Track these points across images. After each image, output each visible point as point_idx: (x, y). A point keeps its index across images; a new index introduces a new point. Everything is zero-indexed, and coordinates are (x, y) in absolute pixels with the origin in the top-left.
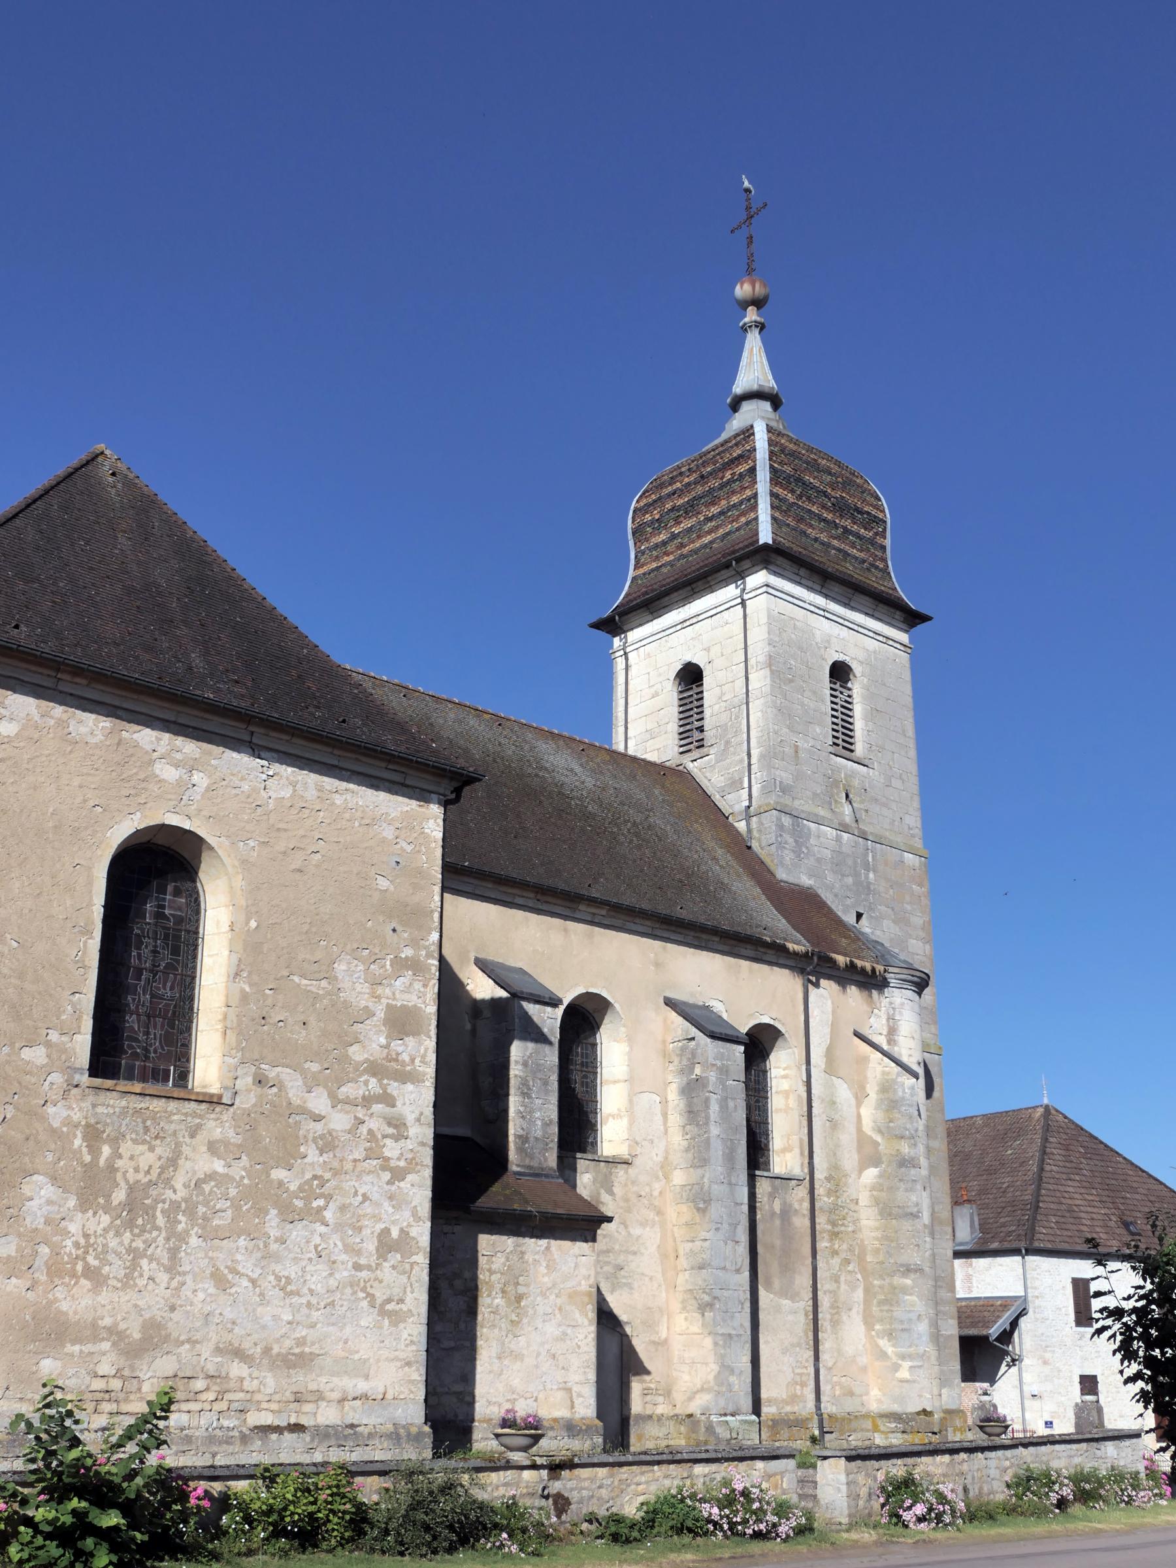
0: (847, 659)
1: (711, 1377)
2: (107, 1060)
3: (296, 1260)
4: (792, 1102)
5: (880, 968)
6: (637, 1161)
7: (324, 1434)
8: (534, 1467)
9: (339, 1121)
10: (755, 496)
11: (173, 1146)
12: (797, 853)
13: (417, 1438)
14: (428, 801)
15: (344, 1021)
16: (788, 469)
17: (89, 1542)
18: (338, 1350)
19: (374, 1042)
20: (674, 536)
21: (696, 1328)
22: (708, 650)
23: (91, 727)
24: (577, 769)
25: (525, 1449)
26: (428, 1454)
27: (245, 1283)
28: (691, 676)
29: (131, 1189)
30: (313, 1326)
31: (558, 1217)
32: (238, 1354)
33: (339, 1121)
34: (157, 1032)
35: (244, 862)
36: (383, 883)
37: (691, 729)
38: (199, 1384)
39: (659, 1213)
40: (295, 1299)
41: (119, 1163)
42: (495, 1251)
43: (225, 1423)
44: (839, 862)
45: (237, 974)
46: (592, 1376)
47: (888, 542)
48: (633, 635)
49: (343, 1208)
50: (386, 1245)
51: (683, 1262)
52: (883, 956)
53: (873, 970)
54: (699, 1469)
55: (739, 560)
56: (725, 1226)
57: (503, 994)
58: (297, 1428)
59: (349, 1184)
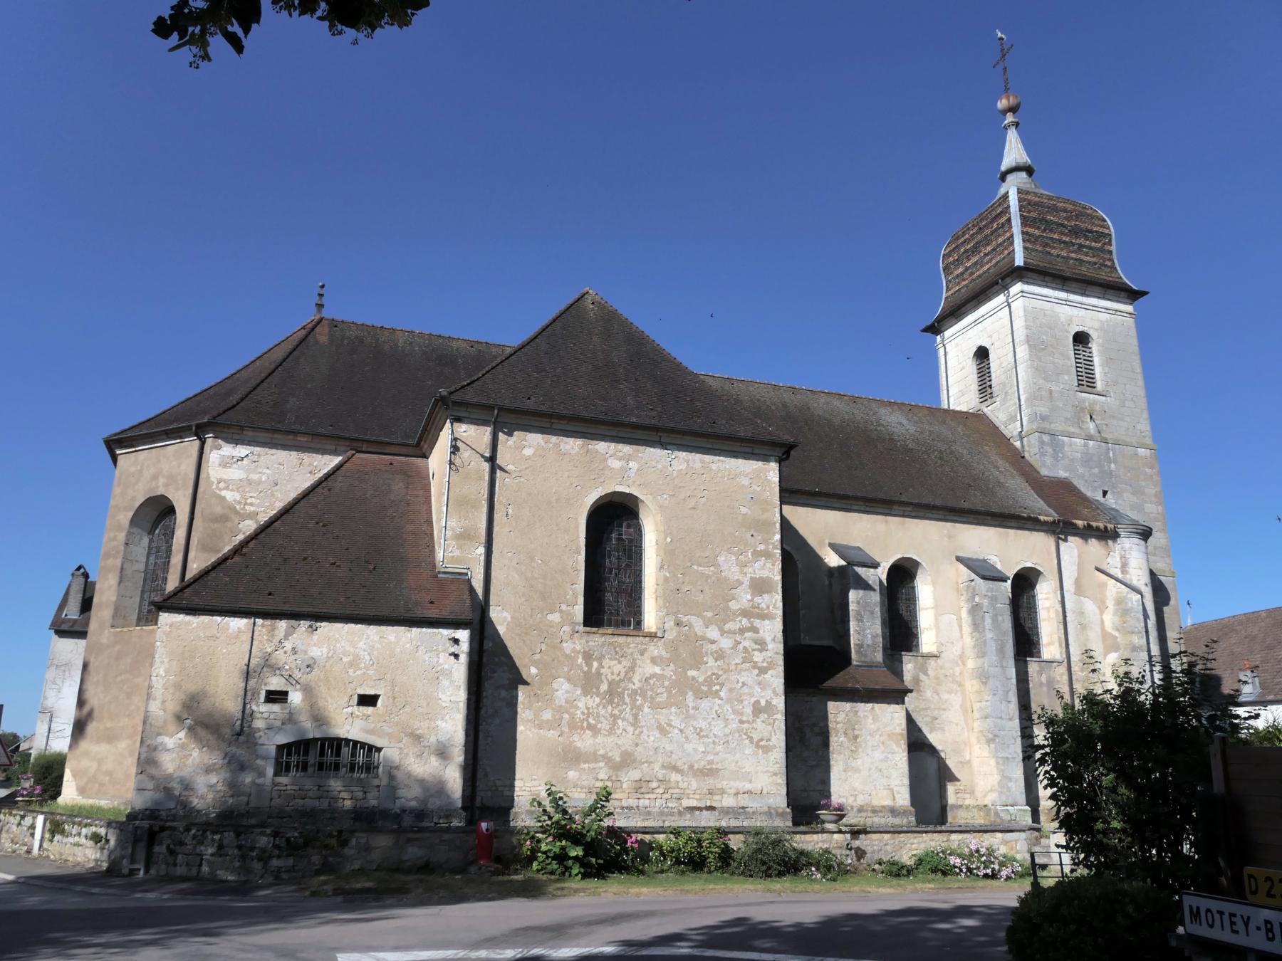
0: (1085, 329)
1: (995, 783)
2: (595, 615)
3: (705, 719)
4: (1052, 615)
5: (1110, 526)
6: (943, 655)
7: (727, 812)
8: (840, 832)
9: (726, 643)
10: (1012, 236)
11: (631, 660)
12: (1056, 458)
13: (782, 815)
14: (768, 461)
15: (726, 588)
16: (1034, 215)
17: (570, 862)
18: (733, 767)
19: (744, 598)
20: (967, 269)
21: (986, 754)
22: (990, 337)
23: (572, 445)
24: (904, 422)
25: (835, 822)
26: (790, 824)
27: (676, 731)
28: (982, 354)
29: (610, 684)
30: (717, 754)
31: (876, 690)
32: (675, 768)
33: (726, 643)
34: (622, 601)
35: (661, 507)
36: (744, 510)
37: (985, 388)
38: (654, 785)
39: (960, 685)
40: (706, 740)
41: (603, 671)
42: (838, 712)
43: (670, 805)
44: (1087, 459)
45: (661, 567)
46: (906, 782)
47: (1113, 248)
48: (947, 333)
49: (731, 690)
50: (757, 710)
51: (976, 715)
52: (1115, 516)
53: (1106, 528)
54: (954, 837)
55: (1003, 279)
56: (1000, 692)
57: (843, 563)
58: (711, 808)
59: (734, 677)
